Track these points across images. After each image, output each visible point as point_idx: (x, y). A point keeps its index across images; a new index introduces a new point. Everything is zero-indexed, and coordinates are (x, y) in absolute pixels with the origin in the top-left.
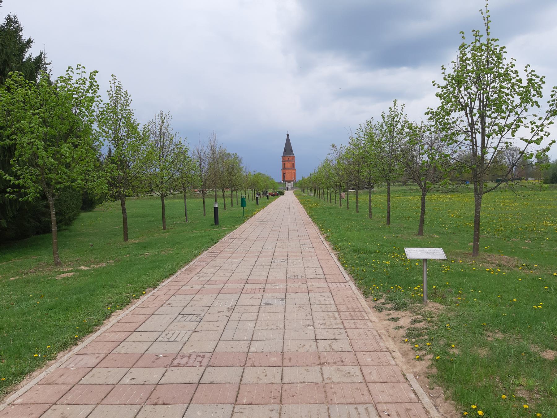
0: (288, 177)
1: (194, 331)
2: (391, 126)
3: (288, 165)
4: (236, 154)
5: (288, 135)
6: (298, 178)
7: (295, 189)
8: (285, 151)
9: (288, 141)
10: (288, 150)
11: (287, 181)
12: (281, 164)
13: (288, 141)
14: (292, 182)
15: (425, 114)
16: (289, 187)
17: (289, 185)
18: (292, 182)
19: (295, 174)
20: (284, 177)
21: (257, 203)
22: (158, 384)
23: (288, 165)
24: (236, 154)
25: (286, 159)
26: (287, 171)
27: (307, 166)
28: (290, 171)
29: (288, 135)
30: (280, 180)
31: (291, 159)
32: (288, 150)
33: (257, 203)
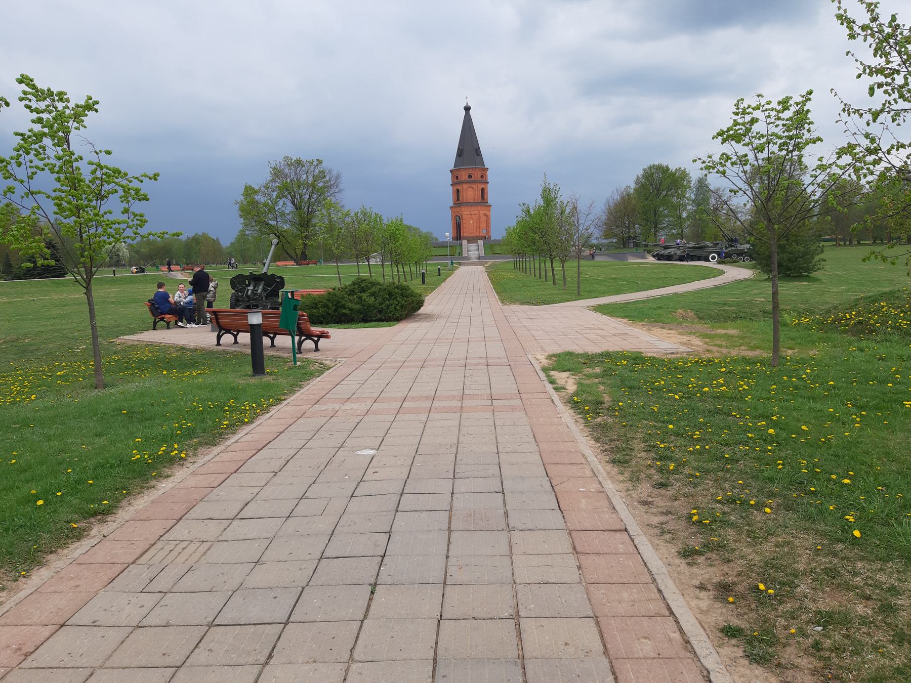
0: (469, 227)
1: (211, 625)
2: (134, 471)
3: (470, 193)
4: (320, 162)
5: (467, 109)
6: (498, 233)
7: (490, 262)
8: (460, 153)
9: (468, 125)
10: (469, 148)
11: (466, 238)
12: (450, 191)
13: (468, 125)
14: (481, 242)
15: (713, 138)
16: (474, 254)
17: (472, 250)
18: (481, 242)
19: (487, 217)
20: (458, 227)
21: (423, 282)
22: (211, 625)
23: (470, 193)
24: (320, 162)
25: (464, 176)
26: (465, 212)
27: (508, 204)
28: (475, 210)
29: (467, 109)
30: (448, 235)
31: (476, 175)
32: (469, 148)
33: (423, 282)
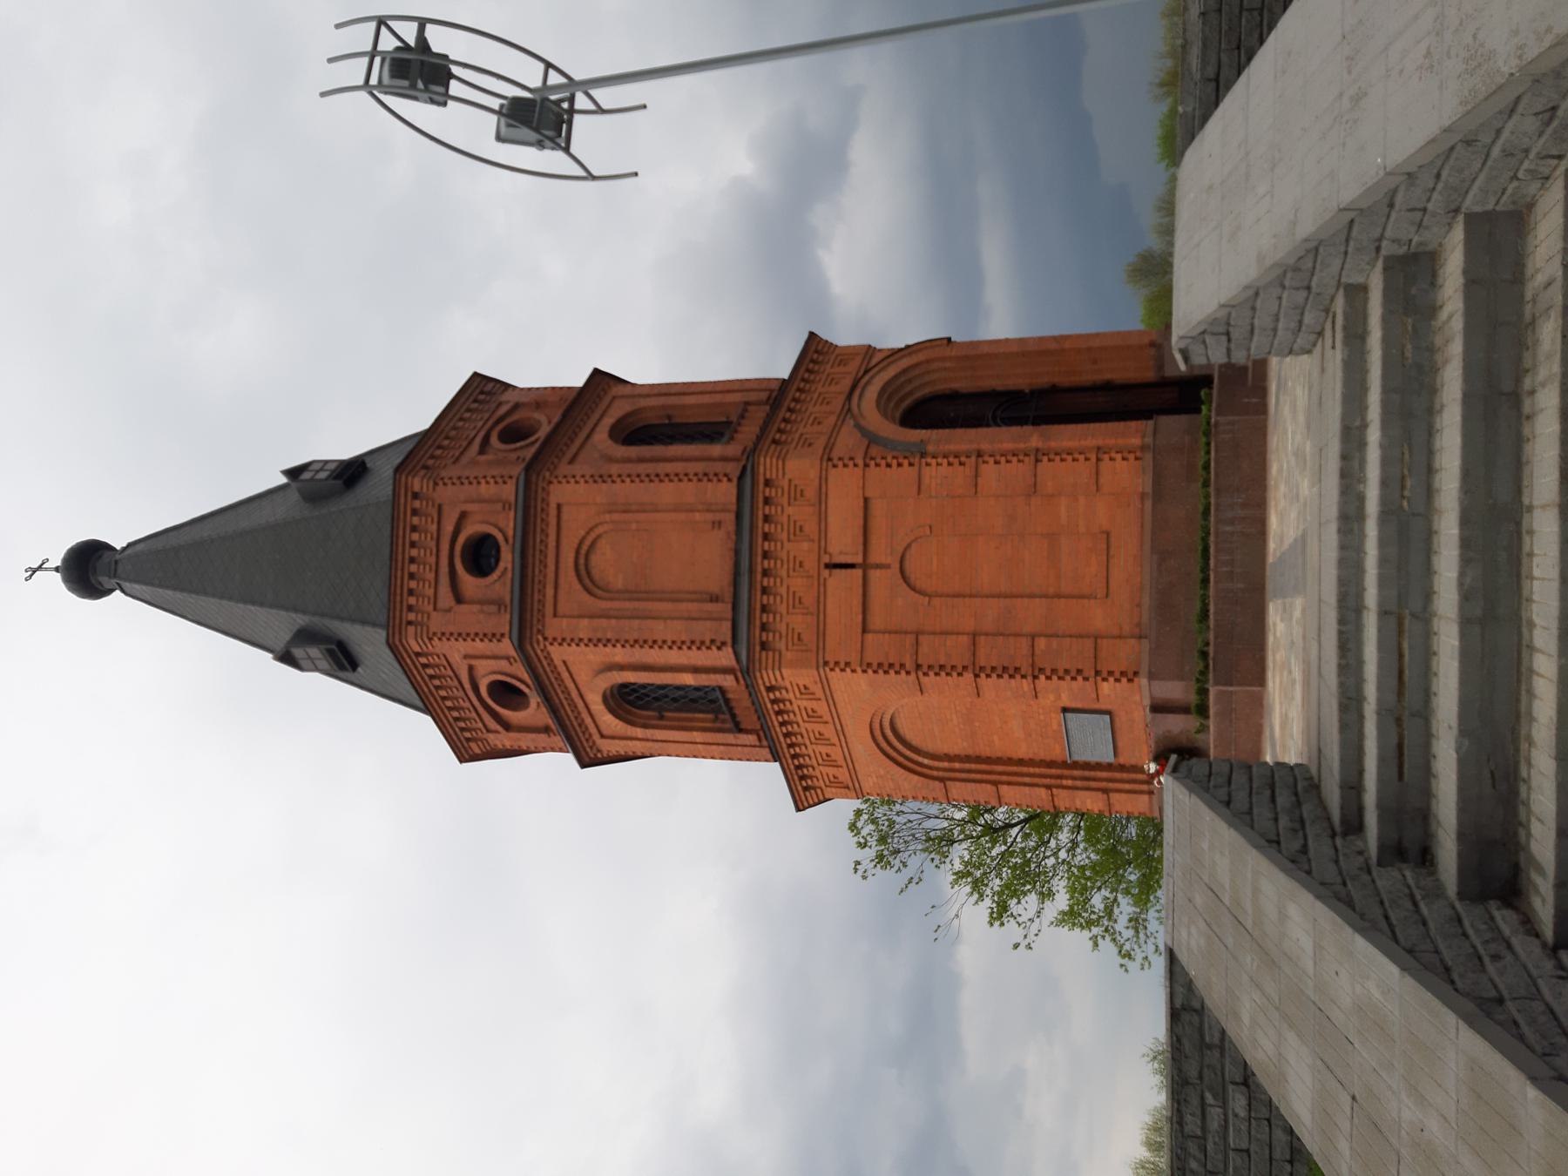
5: (89, 568)
29: (89, 568)
